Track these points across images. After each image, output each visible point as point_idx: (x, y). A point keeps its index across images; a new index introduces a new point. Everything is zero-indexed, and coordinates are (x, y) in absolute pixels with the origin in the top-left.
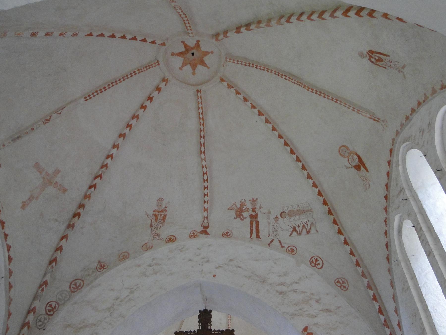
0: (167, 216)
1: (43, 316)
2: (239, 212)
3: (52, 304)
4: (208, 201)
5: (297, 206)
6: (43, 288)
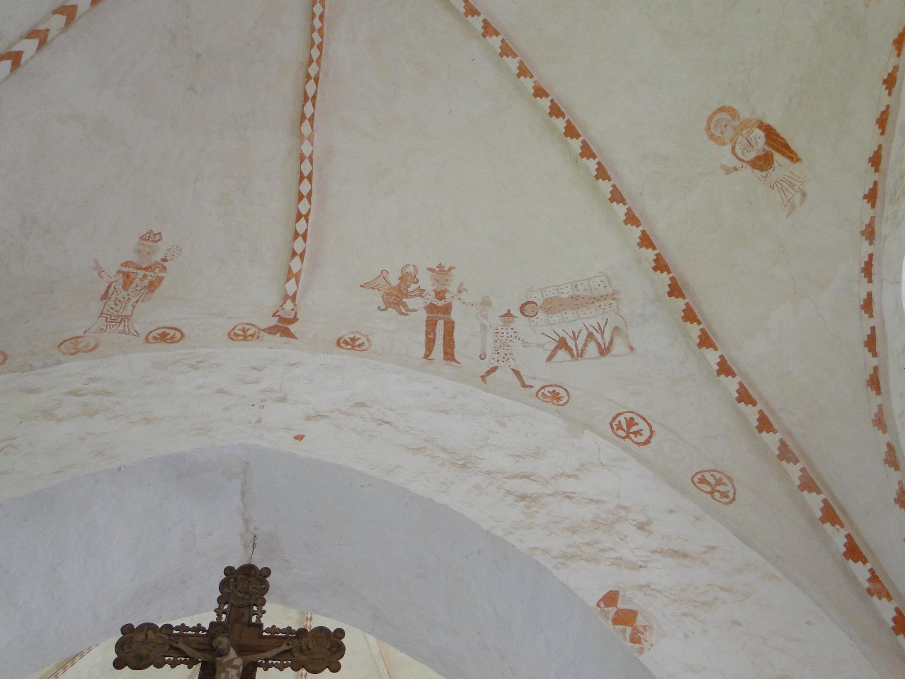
0: (164, 282)
2: (395, 296)
4: (304, 251)
5: (572, 285)
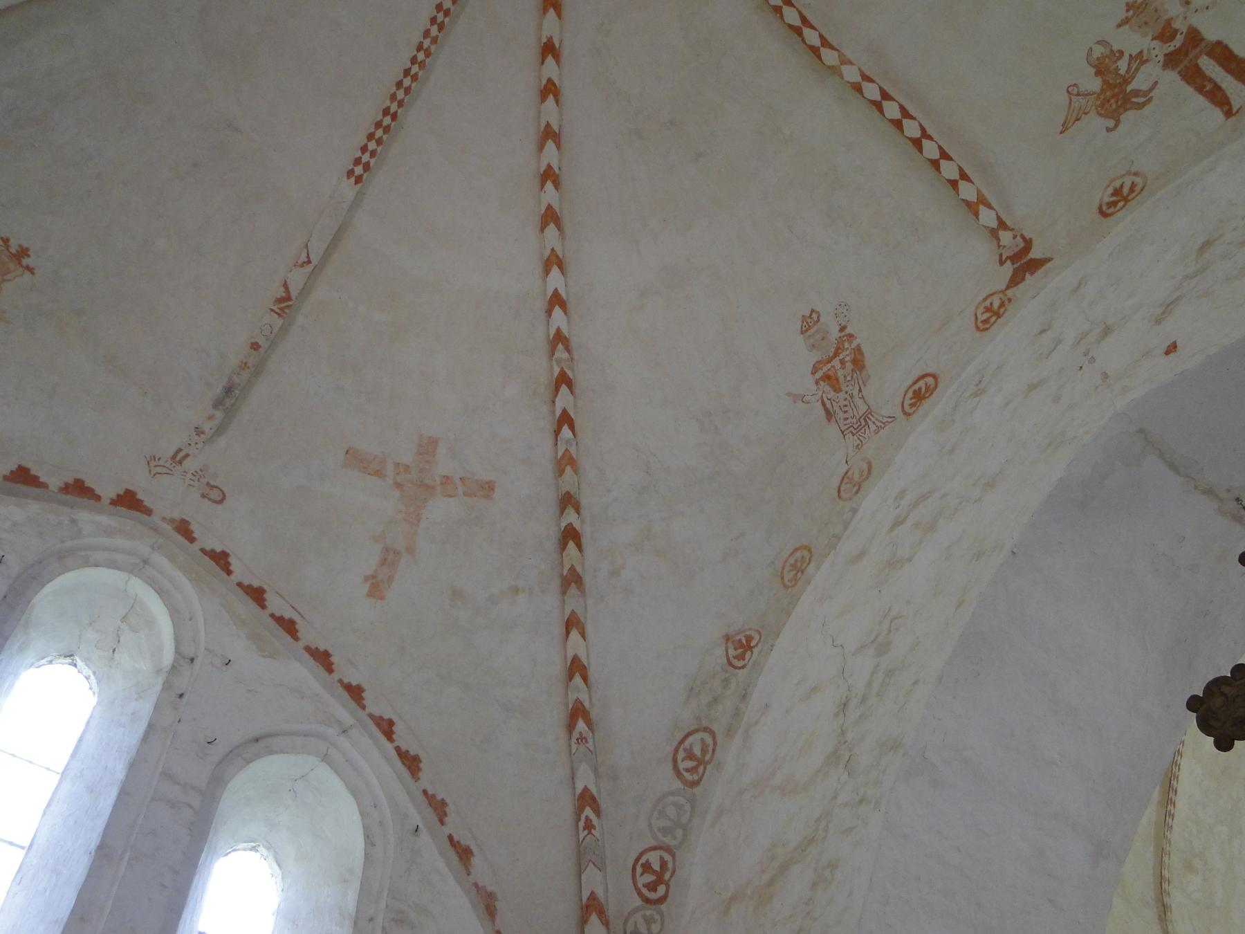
0: (865, 349)
1: (638, 918)
3: (647, 861)
6: (587, 817)
